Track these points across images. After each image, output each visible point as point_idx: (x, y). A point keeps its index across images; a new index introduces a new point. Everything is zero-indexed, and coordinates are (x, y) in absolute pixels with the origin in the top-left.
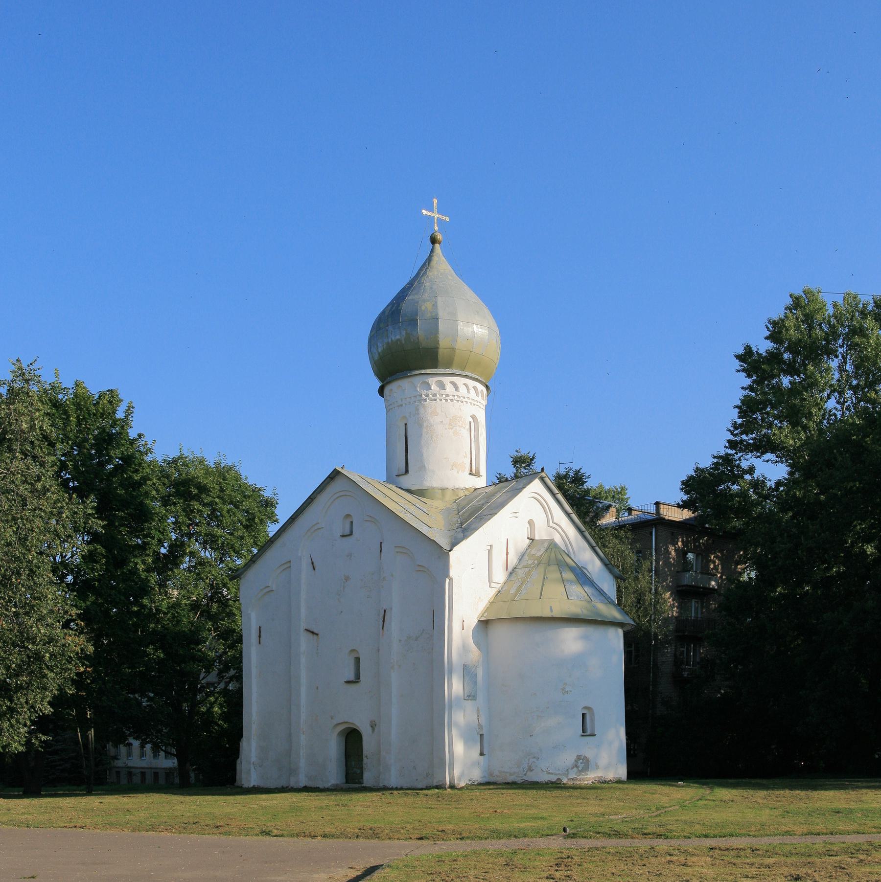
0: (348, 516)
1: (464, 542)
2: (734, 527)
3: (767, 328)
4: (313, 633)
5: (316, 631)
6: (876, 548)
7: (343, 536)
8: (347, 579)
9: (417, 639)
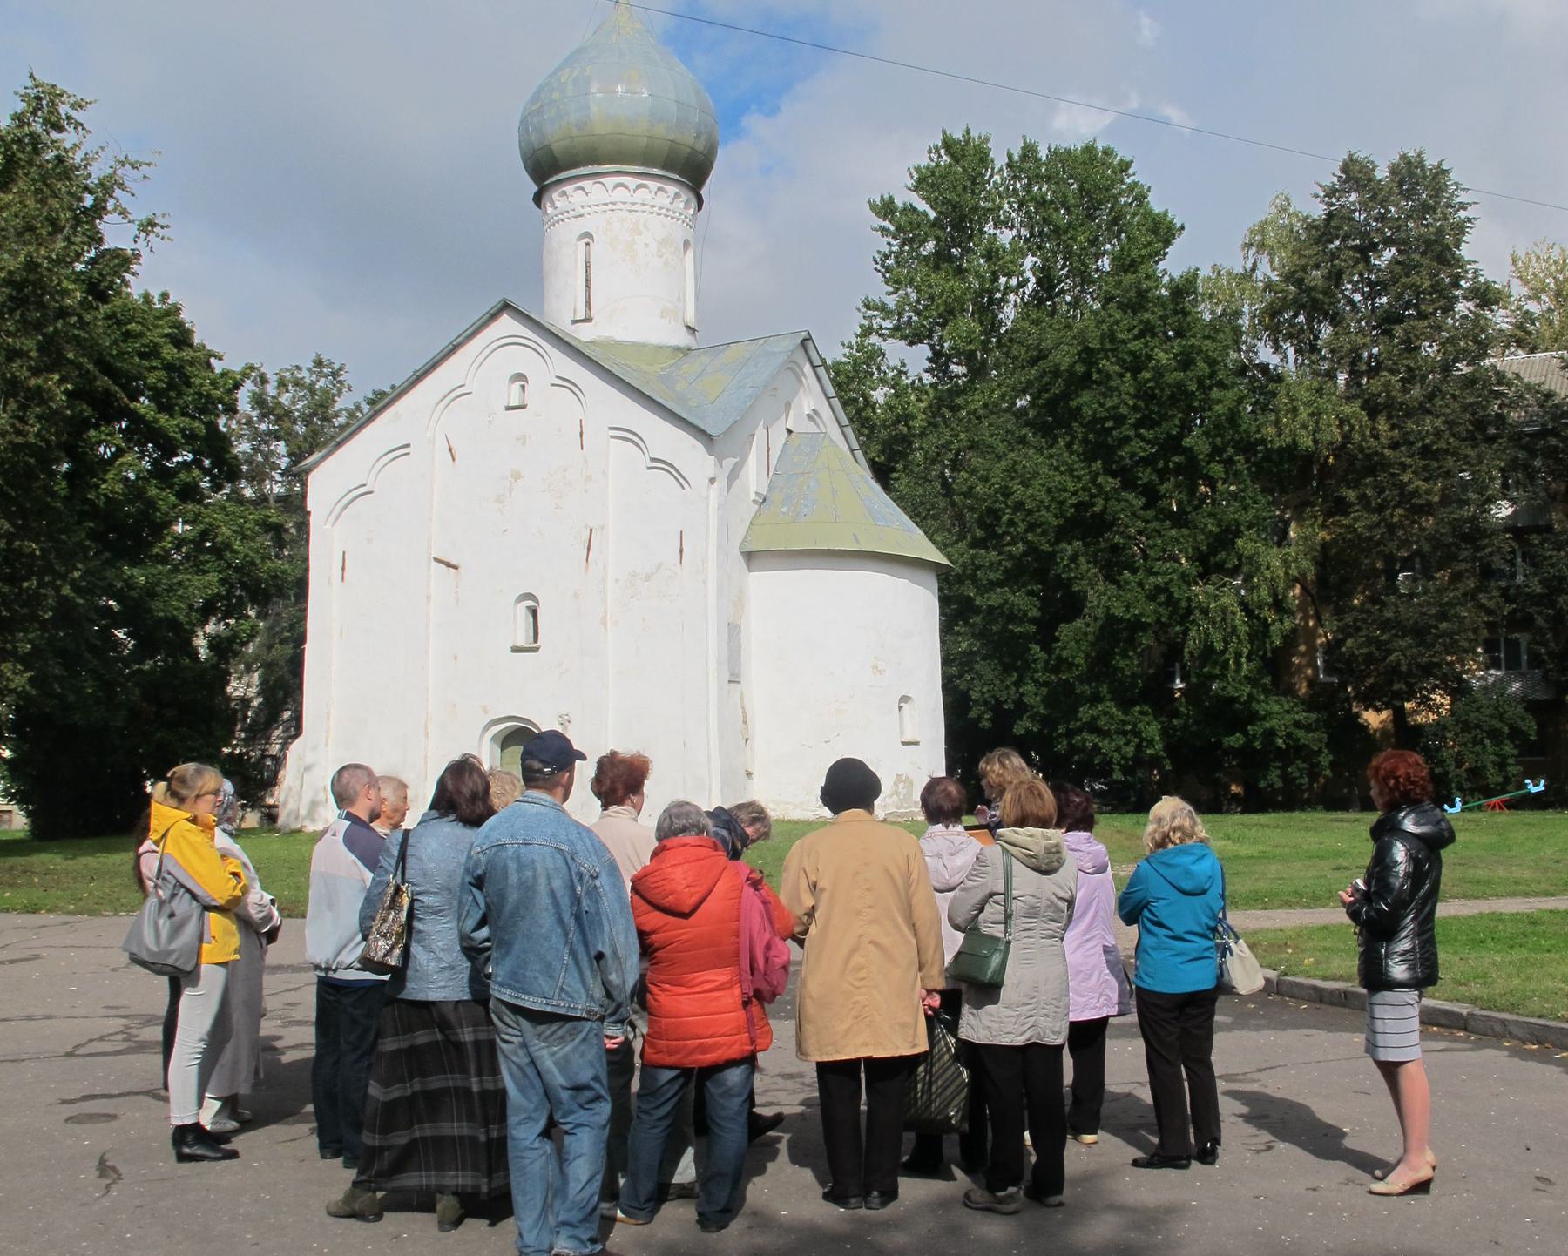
0: (521, 377)
1: (309, 647)
2: (1378, 710)
3: (883, 229)
4: (448, 565)
5: (454, 562)
6: (150, 611)
7: (509, 408)
8: (517, 476)
9: (648, 578)
